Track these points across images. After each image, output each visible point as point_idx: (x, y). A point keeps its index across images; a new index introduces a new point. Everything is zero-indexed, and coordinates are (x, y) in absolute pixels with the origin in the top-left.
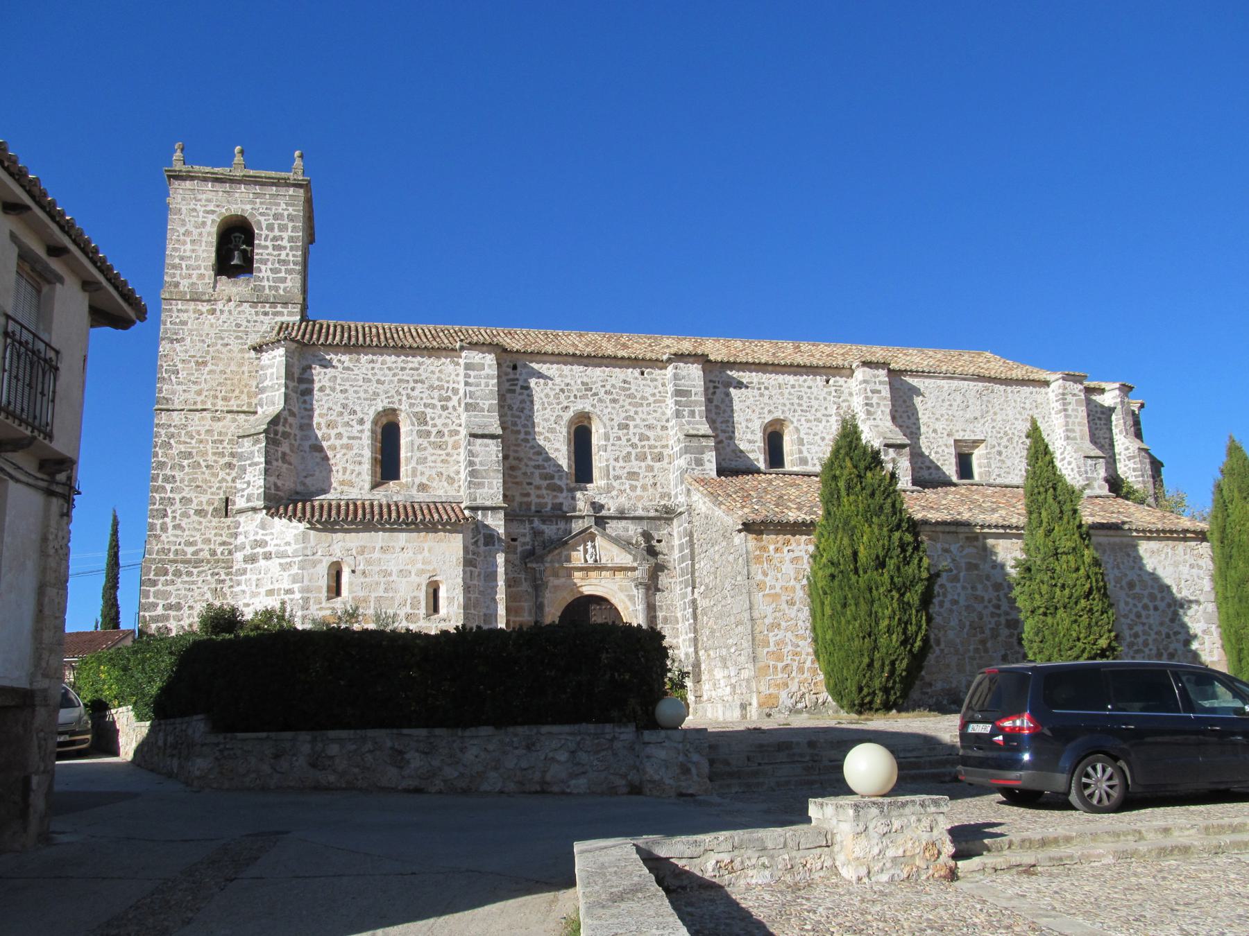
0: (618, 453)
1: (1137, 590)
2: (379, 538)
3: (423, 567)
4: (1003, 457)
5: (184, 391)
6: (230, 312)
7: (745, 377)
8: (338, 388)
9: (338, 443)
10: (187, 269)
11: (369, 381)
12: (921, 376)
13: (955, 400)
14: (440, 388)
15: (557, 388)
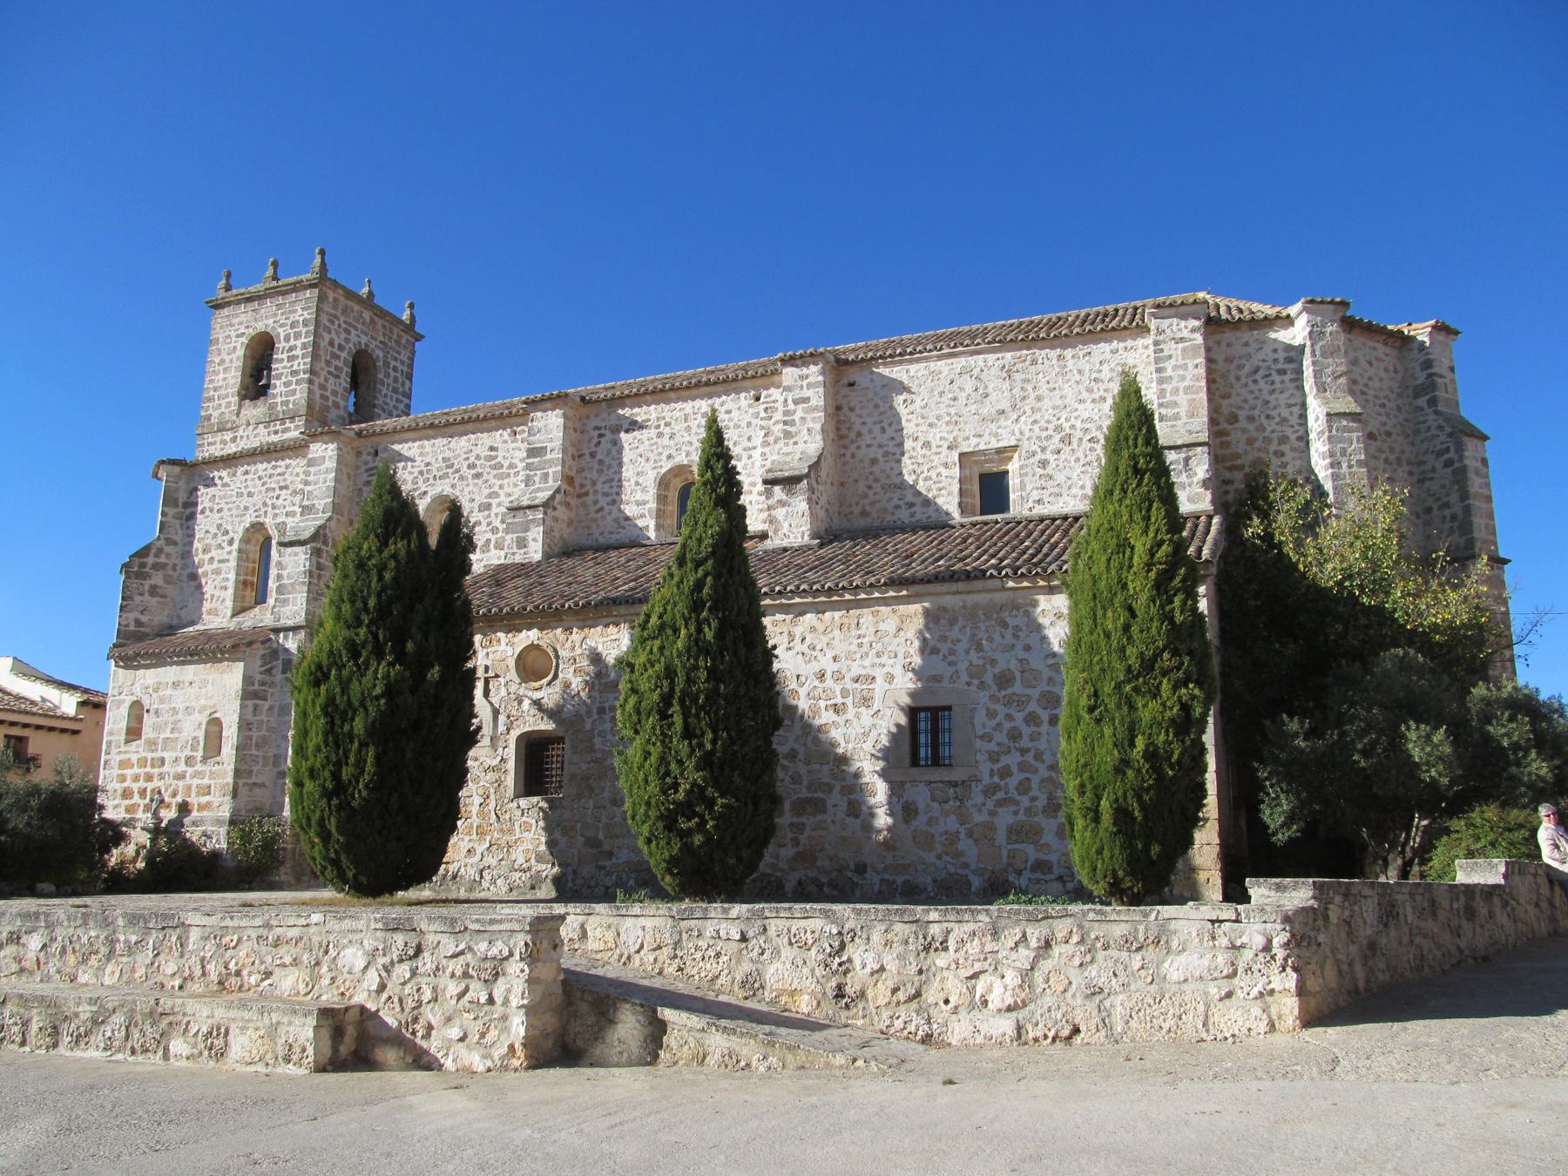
1: (1017, 688)
4: (1049, 470)
7: (640, 413)
11: (242, 495)
12: (901, 362)
13: (962, 389)
15: (416, 470)
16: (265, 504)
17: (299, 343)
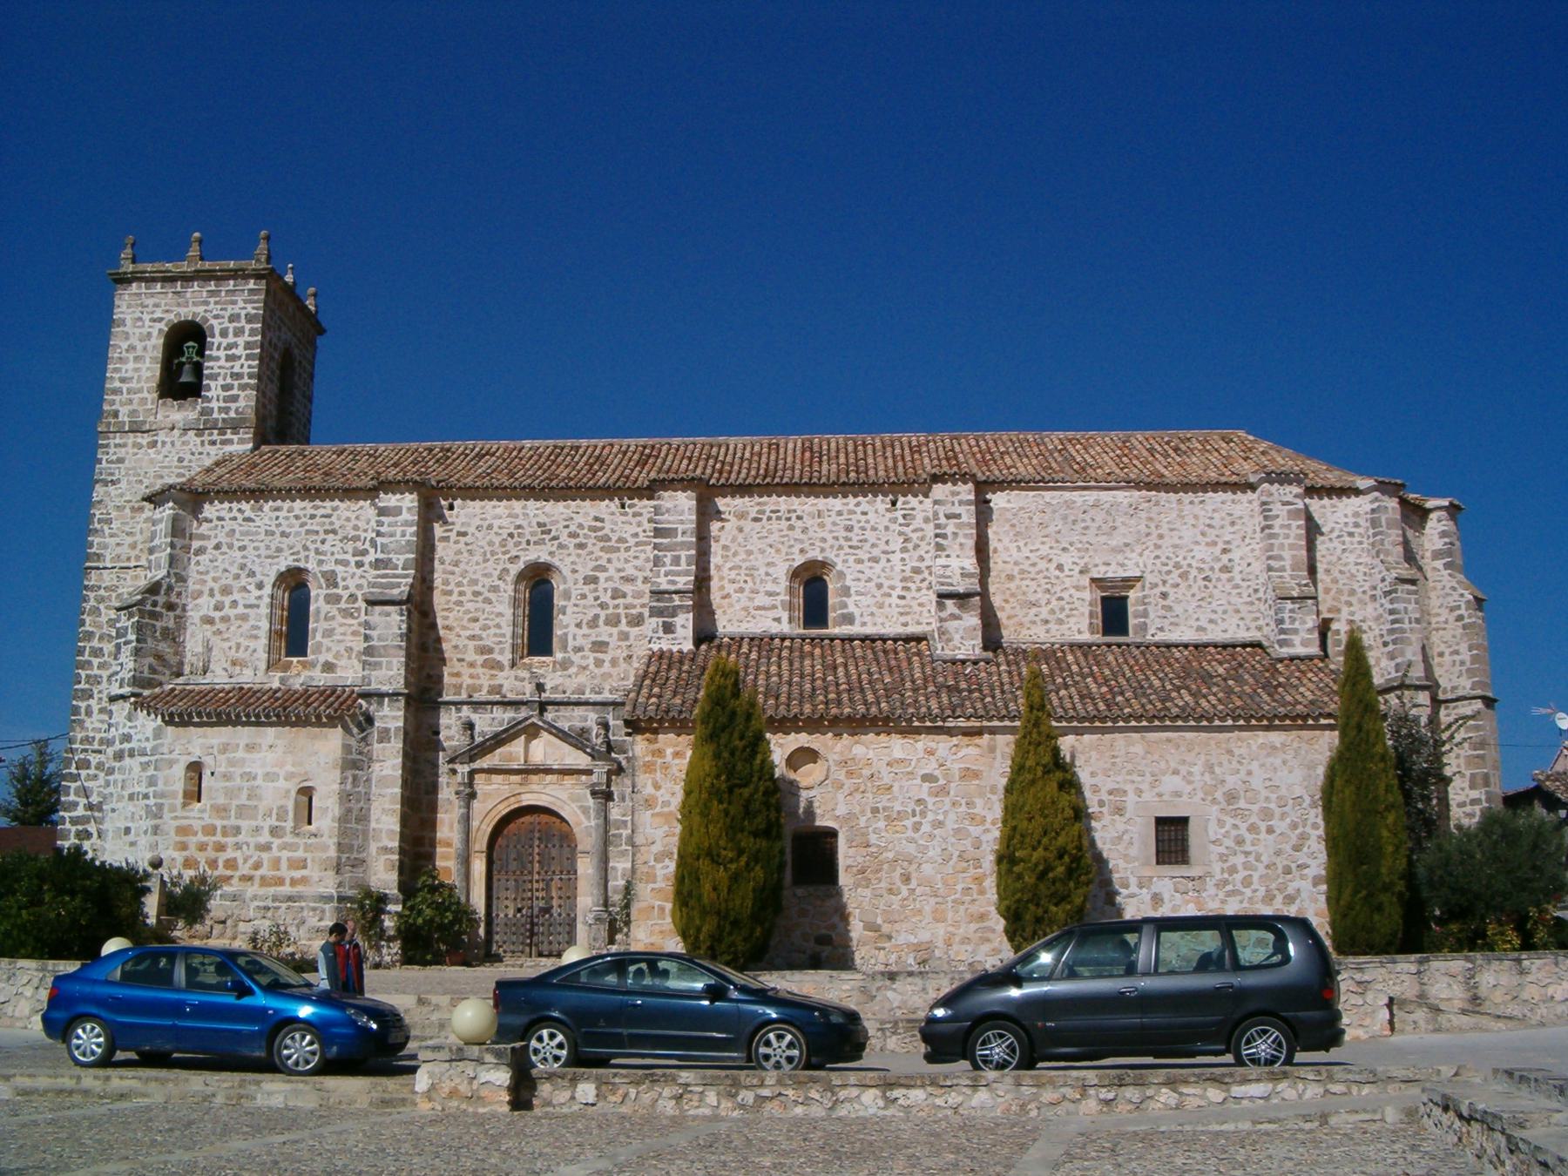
0: (580, 616)
1: (1242, 804)
2: (243, 735)
3: (293, 769)
5: (118, 544)
6: (173, 443)
8: (237, 544)
9: (232, 613)
10: (129, 393)
14: (356, 539)
16: (306, 548)
17: (241, 341)
